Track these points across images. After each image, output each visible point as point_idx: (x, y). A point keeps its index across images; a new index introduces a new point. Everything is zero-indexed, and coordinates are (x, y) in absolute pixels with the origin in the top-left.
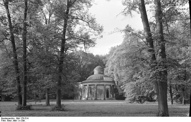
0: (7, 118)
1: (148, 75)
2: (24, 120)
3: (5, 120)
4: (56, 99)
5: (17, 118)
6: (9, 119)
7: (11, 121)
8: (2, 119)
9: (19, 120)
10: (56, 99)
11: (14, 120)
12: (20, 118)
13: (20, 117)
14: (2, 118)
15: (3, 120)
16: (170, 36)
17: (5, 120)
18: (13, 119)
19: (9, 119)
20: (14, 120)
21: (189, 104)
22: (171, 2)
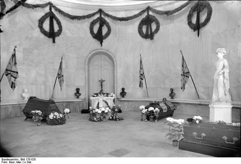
0: (8, 160)
2: (30, 161)
3: (6, 161)
5: (21, 159)
6: (12, 160)
8: (3, 161)
9: (24, 161)
11: (18, 162)
12: (26, 159)
13: (26, 158)
15: (4, 161)
19: (12, 160)
20: (18, 162)
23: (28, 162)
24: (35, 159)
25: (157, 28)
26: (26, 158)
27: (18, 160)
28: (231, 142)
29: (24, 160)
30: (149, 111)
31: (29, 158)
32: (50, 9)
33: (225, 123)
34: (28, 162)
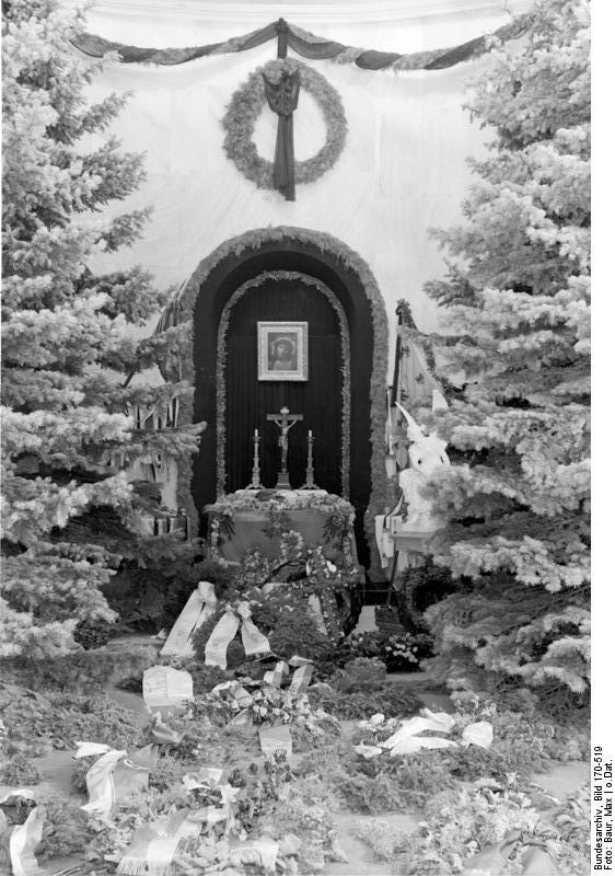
0: (599, 845)
1: (511, 802)
2: (604, 768)
3: (604, 855)
4: (92, 191)
5: (598, 799)
6: (600, 833)
7: (613, 823)
8: (602, 865)
9: (605, 789)
10: (92, 191)
11: (606, 812)
12: (598, 783)
13: (594, 783)
14: (598, 867)
15: (604, 860)
16: (269, 587)
17: (604, 855)
18: (600, 817)
19: (600, 833)
20: (606, 812)
21: (69, 482)
22: (283, 606)
23: (609, 775)
24: (404, 313)
25: (569, 400)
26: (593, 781)
27: (602, 809)
28: (217, 325)
29: (599, 788)
30: (397, 477)
31: (593, 771)
32: (282, 53)
33: (295, 108)
34: (609, 775)
